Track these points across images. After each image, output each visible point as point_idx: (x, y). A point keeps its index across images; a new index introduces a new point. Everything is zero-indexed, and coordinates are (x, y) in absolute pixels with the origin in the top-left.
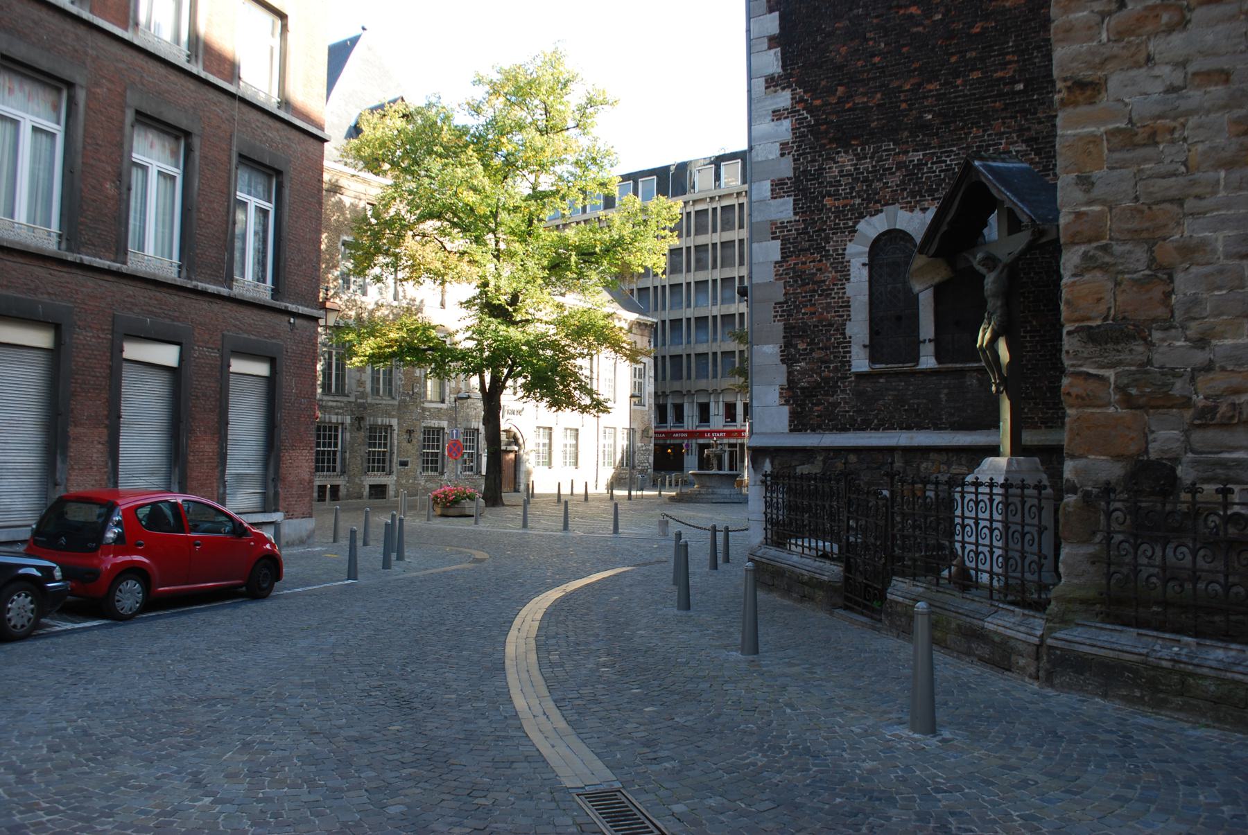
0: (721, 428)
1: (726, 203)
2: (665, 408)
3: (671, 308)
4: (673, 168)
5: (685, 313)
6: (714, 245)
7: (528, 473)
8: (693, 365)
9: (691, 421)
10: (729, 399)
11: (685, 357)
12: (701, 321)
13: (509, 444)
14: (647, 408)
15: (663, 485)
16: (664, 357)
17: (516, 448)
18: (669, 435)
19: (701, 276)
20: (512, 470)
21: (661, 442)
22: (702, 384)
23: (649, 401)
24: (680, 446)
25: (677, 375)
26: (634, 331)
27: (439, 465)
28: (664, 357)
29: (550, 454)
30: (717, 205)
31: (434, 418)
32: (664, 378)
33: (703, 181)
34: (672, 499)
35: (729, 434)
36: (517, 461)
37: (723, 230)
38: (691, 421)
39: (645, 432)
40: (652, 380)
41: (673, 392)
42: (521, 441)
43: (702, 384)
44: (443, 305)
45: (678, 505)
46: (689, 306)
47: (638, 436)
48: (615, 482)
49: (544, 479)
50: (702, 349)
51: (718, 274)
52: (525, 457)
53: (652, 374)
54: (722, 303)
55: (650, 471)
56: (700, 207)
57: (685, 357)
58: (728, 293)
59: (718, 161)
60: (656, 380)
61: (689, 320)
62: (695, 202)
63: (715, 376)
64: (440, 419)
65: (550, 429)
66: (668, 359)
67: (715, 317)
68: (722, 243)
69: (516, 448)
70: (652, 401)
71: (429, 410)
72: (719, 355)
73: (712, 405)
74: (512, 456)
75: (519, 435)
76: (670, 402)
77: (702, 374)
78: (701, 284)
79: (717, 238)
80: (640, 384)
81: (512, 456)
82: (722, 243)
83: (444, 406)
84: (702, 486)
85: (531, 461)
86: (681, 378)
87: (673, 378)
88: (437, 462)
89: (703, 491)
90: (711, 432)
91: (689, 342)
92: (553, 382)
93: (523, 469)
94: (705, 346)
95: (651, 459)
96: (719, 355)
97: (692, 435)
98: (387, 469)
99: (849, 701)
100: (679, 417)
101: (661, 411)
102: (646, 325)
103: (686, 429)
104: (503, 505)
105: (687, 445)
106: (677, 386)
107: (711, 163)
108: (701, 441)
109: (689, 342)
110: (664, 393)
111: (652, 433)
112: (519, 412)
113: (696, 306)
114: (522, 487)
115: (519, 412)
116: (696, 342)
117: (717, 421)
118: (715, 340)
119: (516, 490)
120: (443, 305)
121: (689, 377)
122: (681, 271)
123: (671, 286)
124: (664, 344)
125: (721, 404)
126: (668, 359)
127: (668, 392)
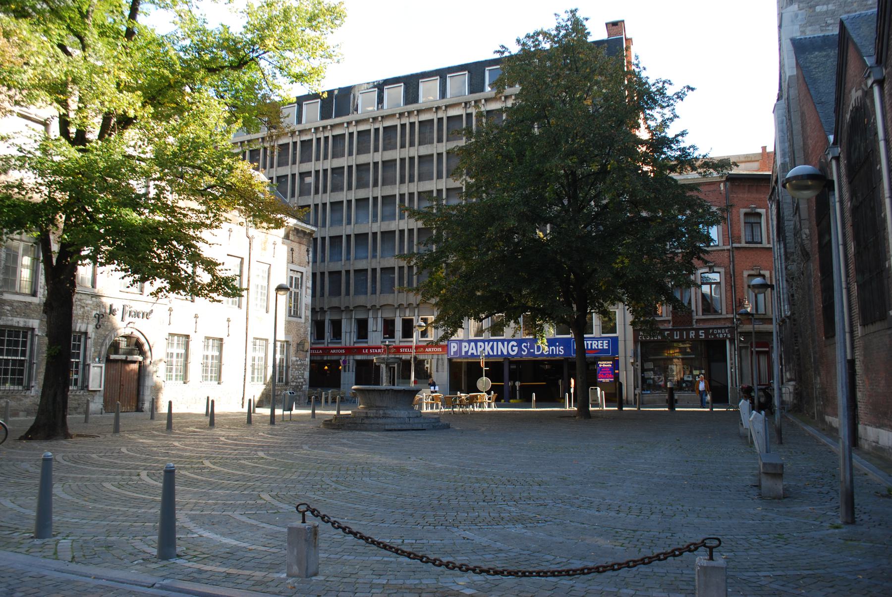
0: (379, 344)
1: (388, 123)
2: (323, 324)
3: (331, 225)
4: (336, 92)
5: (345, 230)
6: (376, 164)
7: (157, 389)
8: (352, 281)
9: (349, 338)
10: (388, 315)
11: (344, 273)
12: (361, 238)
13: (131, 353)
14: (303, 320)
15: (318, 401)
16: (323, 274)
17: (140, 358)
18: (326, 351)
19: (362, 194)
20: (134, 385)
21: (319, 358)
22: (361, 300)
23: (306, 313)
24: (337, 363)
25: (336, 291)
26: (291, 237)
27: (25, 377)
28: (323, 274)
29: (186, 366)
30: (380, 125)
31: (19, 315)
32: (322, 295)
33: (366, 105)
34: (337, 425)
35: (388, 349)
36: (142, 372)
37: (385, 149)
38: (349, 338)
39: (300, 345)
40: (310, 291)
41: (331, 308)
42: (146, 347)
43: (361, 300)
44: (228, 320)
45: (345, 436)
46: (349, 223)
47: (292, 349)
48: (269, 399)
49: (179, 395)
50: (361, 265)
51: (379, 192)
52: (151, 368)
53: (310, 284)
54: (383, 220)
55: (305, 387)
56: (362, 128)
57: (344, 273)
58: (388, 209)
59: (381, 86)
60: (314, 295)
61: (348, 236)
62: (358, 122)
63: (374, 292)
64: (28, 316)
65: (187, 336)
66: (327, 275)
67: (375, 234)
68: (383, 162)
69: (140, 358)
70: (309, 313)
71: (10, 303)
72: (378, 271)
73: (371, 322)
74: (135, 367)
75: (143, 340)
76: (328, 318)
77: (361, 289)
78: (362, 202)
79: (378, 157)
80: (296, 294)
81: (135, 367)
82: (383, 162)
83: (35, 300)
84: (369, 406)
85: (158, 374)
86: (340, 294)
87: (331, 294)
88: (21, 372)
89: (372, 413)
90: (369, 348)
91: (348, 259)
92: (156, 253)
93: (148, 383)
94: (364, 262)
95: (307, 374)
96: (378, 271)
97: (349, 351)
98: (25, 382)
99: (378, 469)
100: (337, 333)
101: (318, 327)
102: (304, 233)
103: (343, 345)
104: (67, 436)
105: (344, 362)
106: (335, 302)
107: (374, 87)
108: (359, 357)
109: (348, 259)
110: (322, 309)
111: (308, 346)
112: (146, 315)
113: (356, 223)
114: (147, 405)
115: (146, 315)
116: (356, 259)
117: (375, 337)
118: (374, 256)
119: (139, 409)
120: (228, 320)
121: (348, 293)
122: (342, 189)
123: (331, 203)
124: (323, 260)
125: (379, 320)
126: (327, 275)
127: (326, 308)
